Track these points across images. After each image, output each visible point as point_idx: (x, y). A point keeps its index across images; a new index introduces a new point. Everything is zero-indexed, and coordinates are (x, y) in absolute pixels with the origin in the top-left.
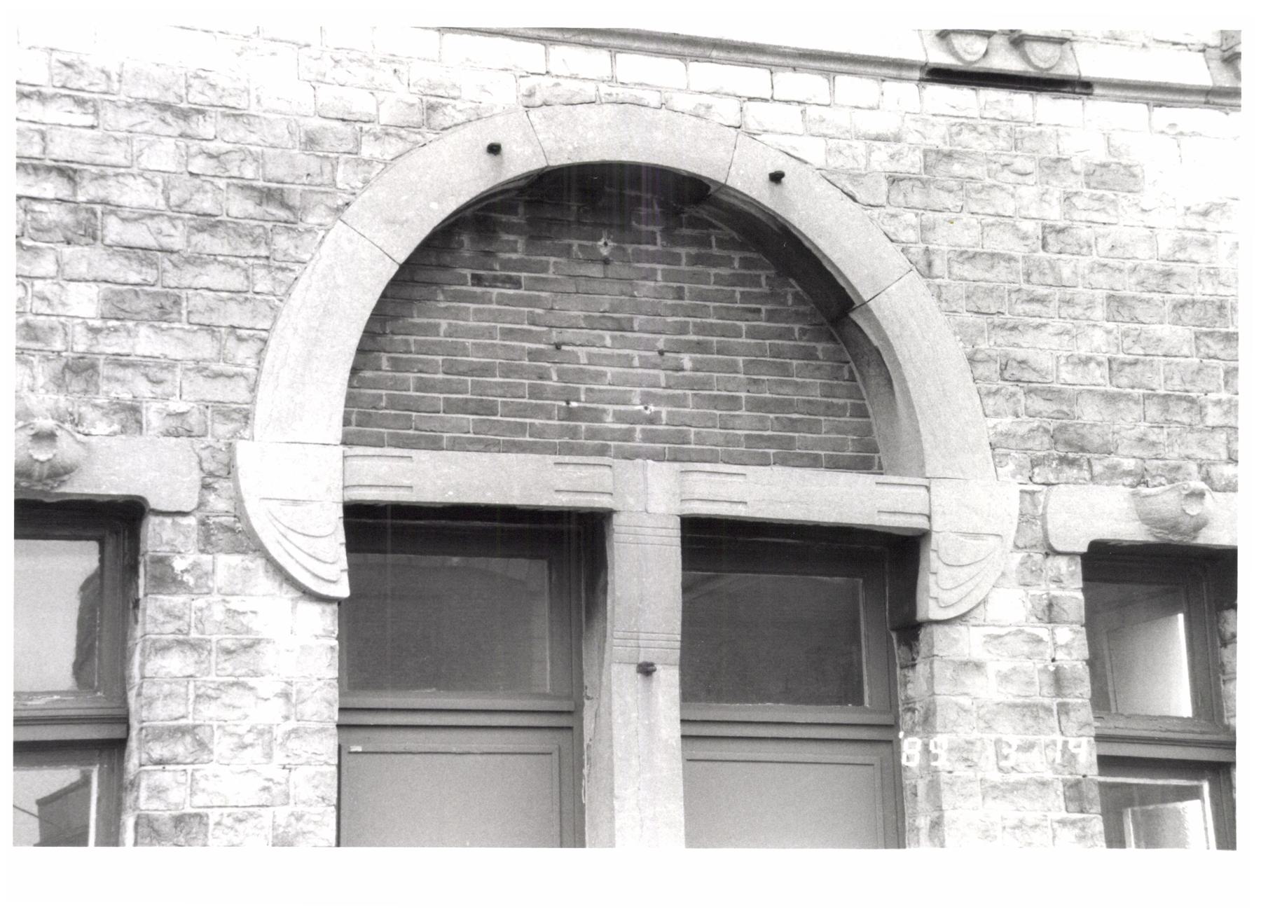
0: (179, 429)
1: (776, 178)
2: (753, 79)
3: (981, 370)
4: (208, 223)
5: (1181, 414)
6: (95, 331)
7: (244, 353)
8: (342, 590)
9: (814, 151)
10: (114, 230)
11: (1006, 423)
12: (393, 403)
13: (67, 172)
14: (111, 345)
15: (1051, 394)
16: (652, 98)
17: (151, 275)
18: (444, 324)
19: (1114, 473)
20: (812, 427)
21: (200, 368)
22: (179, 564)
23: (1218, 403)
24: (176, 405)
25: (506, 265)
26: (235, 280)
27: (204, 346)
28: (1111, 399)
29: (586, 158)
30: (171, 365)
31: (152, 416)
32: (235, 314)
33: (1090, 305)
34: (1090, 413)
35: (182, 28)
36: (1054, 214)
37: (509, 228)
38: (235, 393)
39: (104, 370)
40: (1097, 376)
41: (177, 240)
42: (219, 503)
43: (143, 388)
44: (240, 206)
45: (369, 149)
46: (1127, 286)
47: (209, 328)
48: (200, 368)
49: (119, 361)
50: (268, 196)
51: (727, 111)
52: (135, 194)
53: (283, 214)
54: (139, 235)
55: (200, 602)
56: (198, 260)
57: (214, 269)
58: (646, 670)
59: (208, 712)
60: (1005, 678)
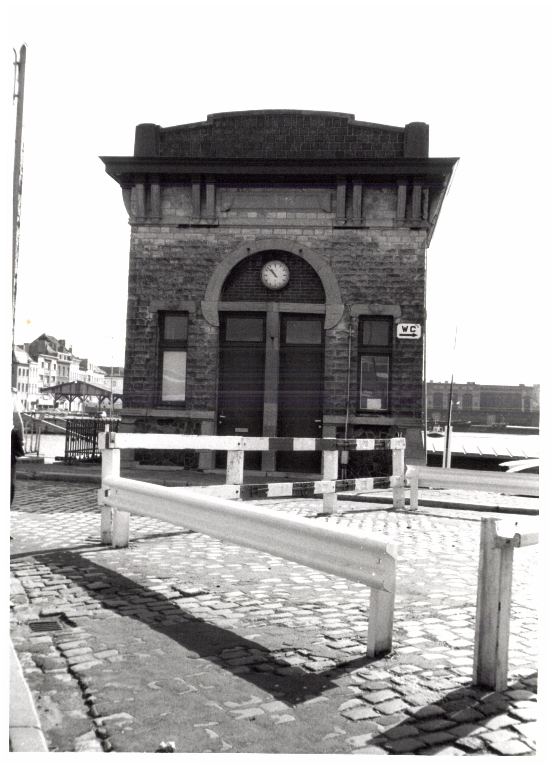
0: (194, 299)
1: (301, 251)
2: (298, 232)
3: (341, 283)
4: (199, 266)
5: (382, 291)
6: (182, 284)
7: (204, 287)
8: (218, 325)
9: (309, 244)
10: (185, 267)
11: (345, 292)
12: (235, 292)
13: (179, 259)
14: (184, 287)
15: (356, 287)
16: (279, 237)
17: (190, 275)
18: (245, 278)
19: (367, 301)
20: (312, 293)
21: (197, 290)
22: (193, 321)
23: (389, 288)
24: (193, 295)
25: (258, 267)
26: (202, 275)
27: (198, 287)
28: (367, 288)
29: (265, 249)
30: (192, 289)
31: (190, 298)
32: (202, 280)
33: (365, 270)
34: (363, 291)
35: (15, 294)
36: (359, 253)
37: (258, 261)
38: (201, 293)
39: (183, 290)
40: (365, 284)
41: (194, 268)
42: (199, 312)
43: (188, 293)
44: (204, 263)
45: (226, 251)
46: (374, 266)
47: (199, 283)
48: (197, 290)
49: (186, 289)
50: (209, 260)
51: (293, 238)
52: (188, 262)
53: (210, 263)
54: (188, 268)
55: (196, 327)
56: (197, 272)
57: (199, 273)
58: (272, 338)
59: (197, 344)
60: (339, 339)
